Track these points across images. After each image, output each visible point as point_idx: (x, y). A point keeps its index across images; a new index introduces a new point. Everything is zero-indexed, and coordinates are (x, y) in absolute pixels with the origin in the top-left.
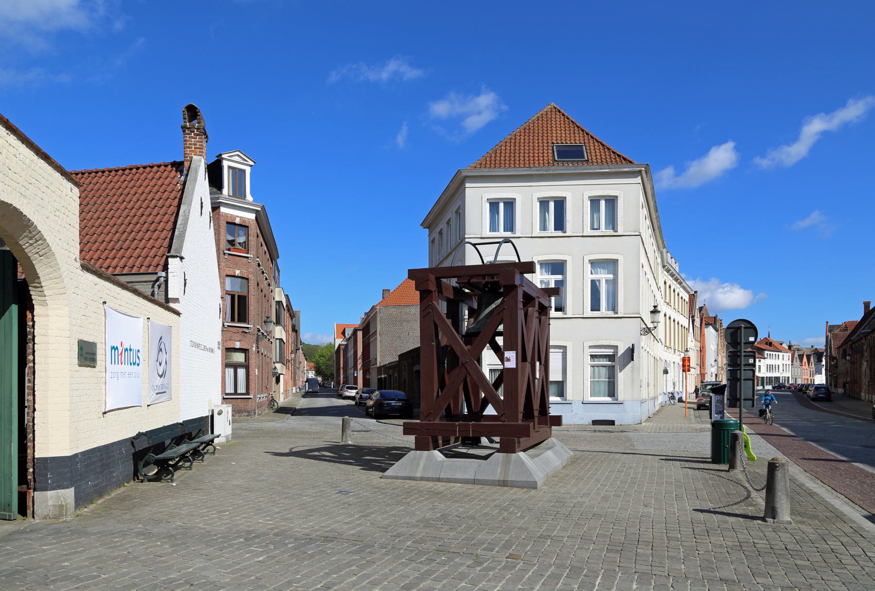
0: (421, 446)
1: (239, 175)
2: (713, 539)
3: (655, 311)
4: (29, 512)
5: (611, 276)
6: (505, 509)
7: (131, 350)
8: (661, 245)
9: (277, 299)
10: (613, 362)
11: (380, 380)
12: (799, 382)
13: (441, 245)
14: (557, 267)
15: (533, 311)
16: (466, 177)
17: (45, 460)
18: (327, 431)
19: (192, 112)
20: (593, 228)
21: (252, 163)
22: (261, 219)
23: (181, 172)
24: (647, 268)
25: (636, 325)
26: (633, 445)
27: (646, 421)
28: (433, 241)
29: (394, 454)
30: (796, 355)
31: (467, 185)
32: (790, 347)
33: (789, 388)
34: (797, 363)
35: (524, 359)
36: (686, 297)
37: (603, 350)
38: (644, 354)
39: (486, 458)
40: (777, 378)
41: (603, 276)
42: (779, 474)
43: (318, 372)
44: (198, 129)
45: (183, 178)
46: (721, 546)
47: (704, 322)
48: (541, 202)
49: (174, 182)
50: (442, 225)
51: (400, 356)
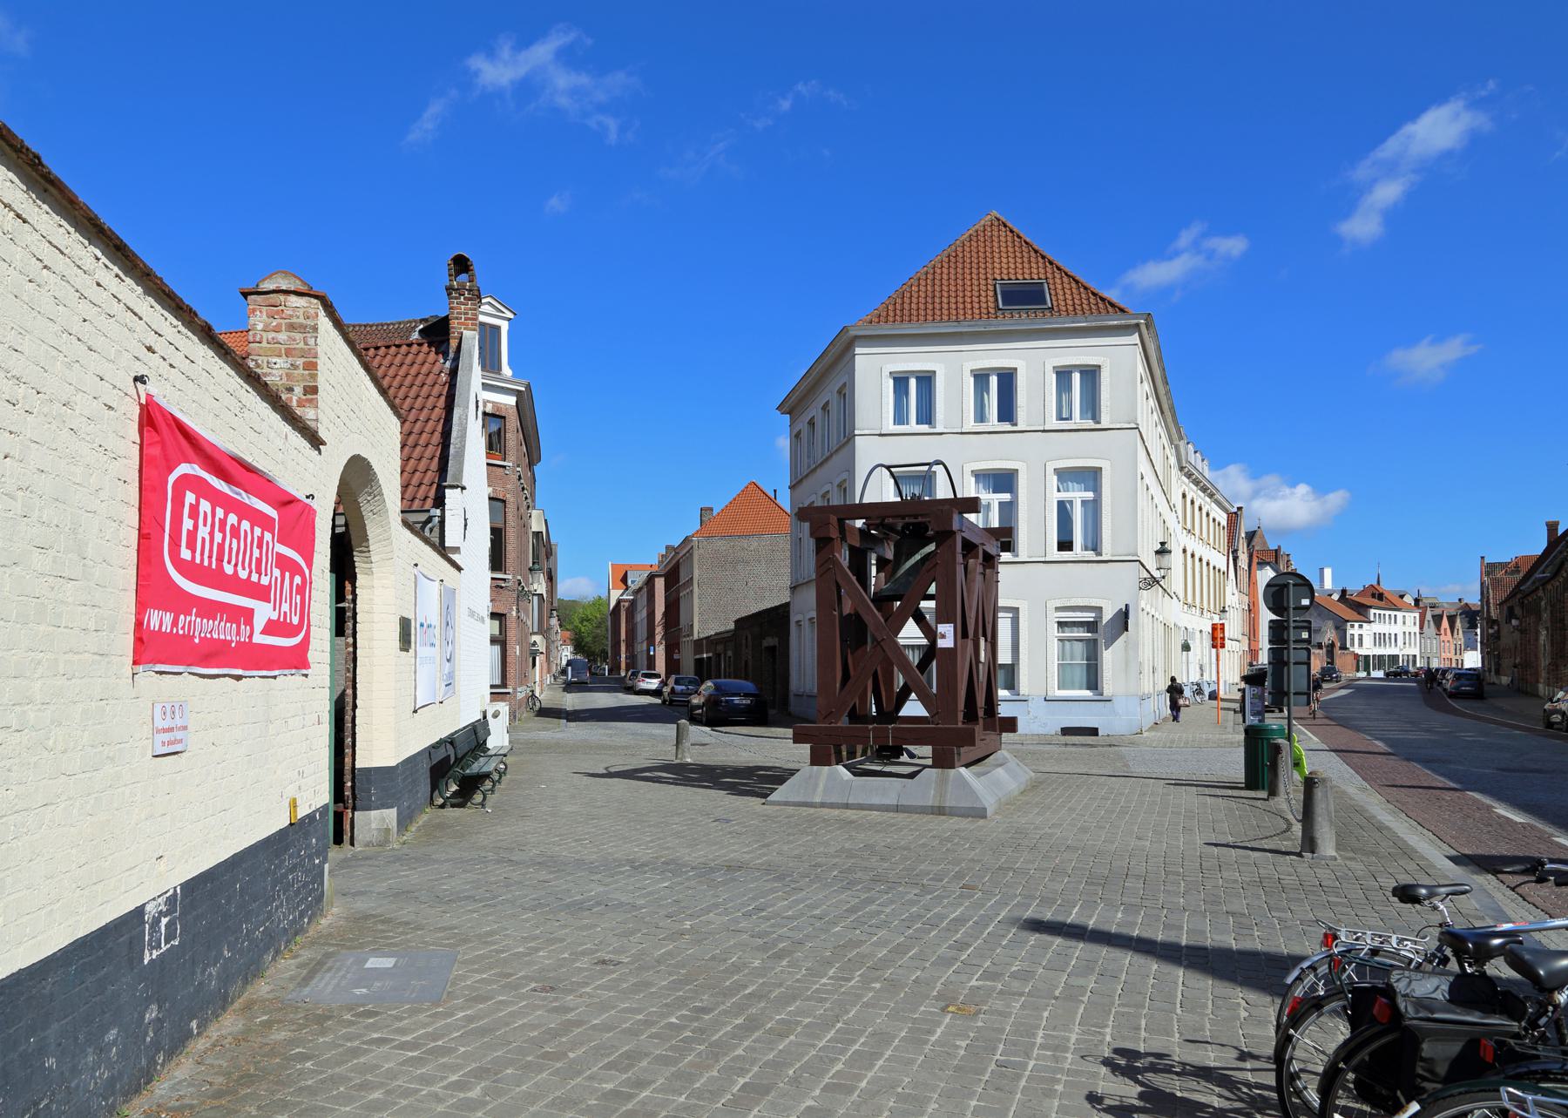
0: (818, 759)
1: (489, 335)
2: (1225, 874)
3: (1163, 551)
4: (346, 838)
5: (1090, 495)
6: (948, 840)
7: (1213, 696)
8: (1175, 436)
9: (535, 528)
10: (1096, 634)
11: (699, 662)
12: (1435, 664)
13: (811, 443)
14: (1003, 481)
15: (975, 564)
16: (857, 337)
17: (368, 770)
18: (655, 741)
19: (461, 264)
20: (1060, 418)
21: (511, 316)
22: (525, 403)
23: (445, 354)
24: (1150, 479)
25: (1131, 573)
26: (1127, 766)
27: (1151, 729)
28: (798, 436)
29: (779, 776)
30: (1429, 616)
31: (858, 350)
32: (1417, 601)
33: (1417, 675)
34: (1430, 629)
35: (965, 635)
36: (1222, 518)
37: (1079, 614)
38: (1145, 620)
39: (912, 776)
40: (1394, 658)
41: (1078, 496)
42: (1319, 793)
43: (579, 646)
44: (470, 290)
45: (448, 364)
46: (1236, 881)
47: (1255, 560)
48: (975, 376)
49: (436, 370)
50: (814, 411)
51: (737, 622)
